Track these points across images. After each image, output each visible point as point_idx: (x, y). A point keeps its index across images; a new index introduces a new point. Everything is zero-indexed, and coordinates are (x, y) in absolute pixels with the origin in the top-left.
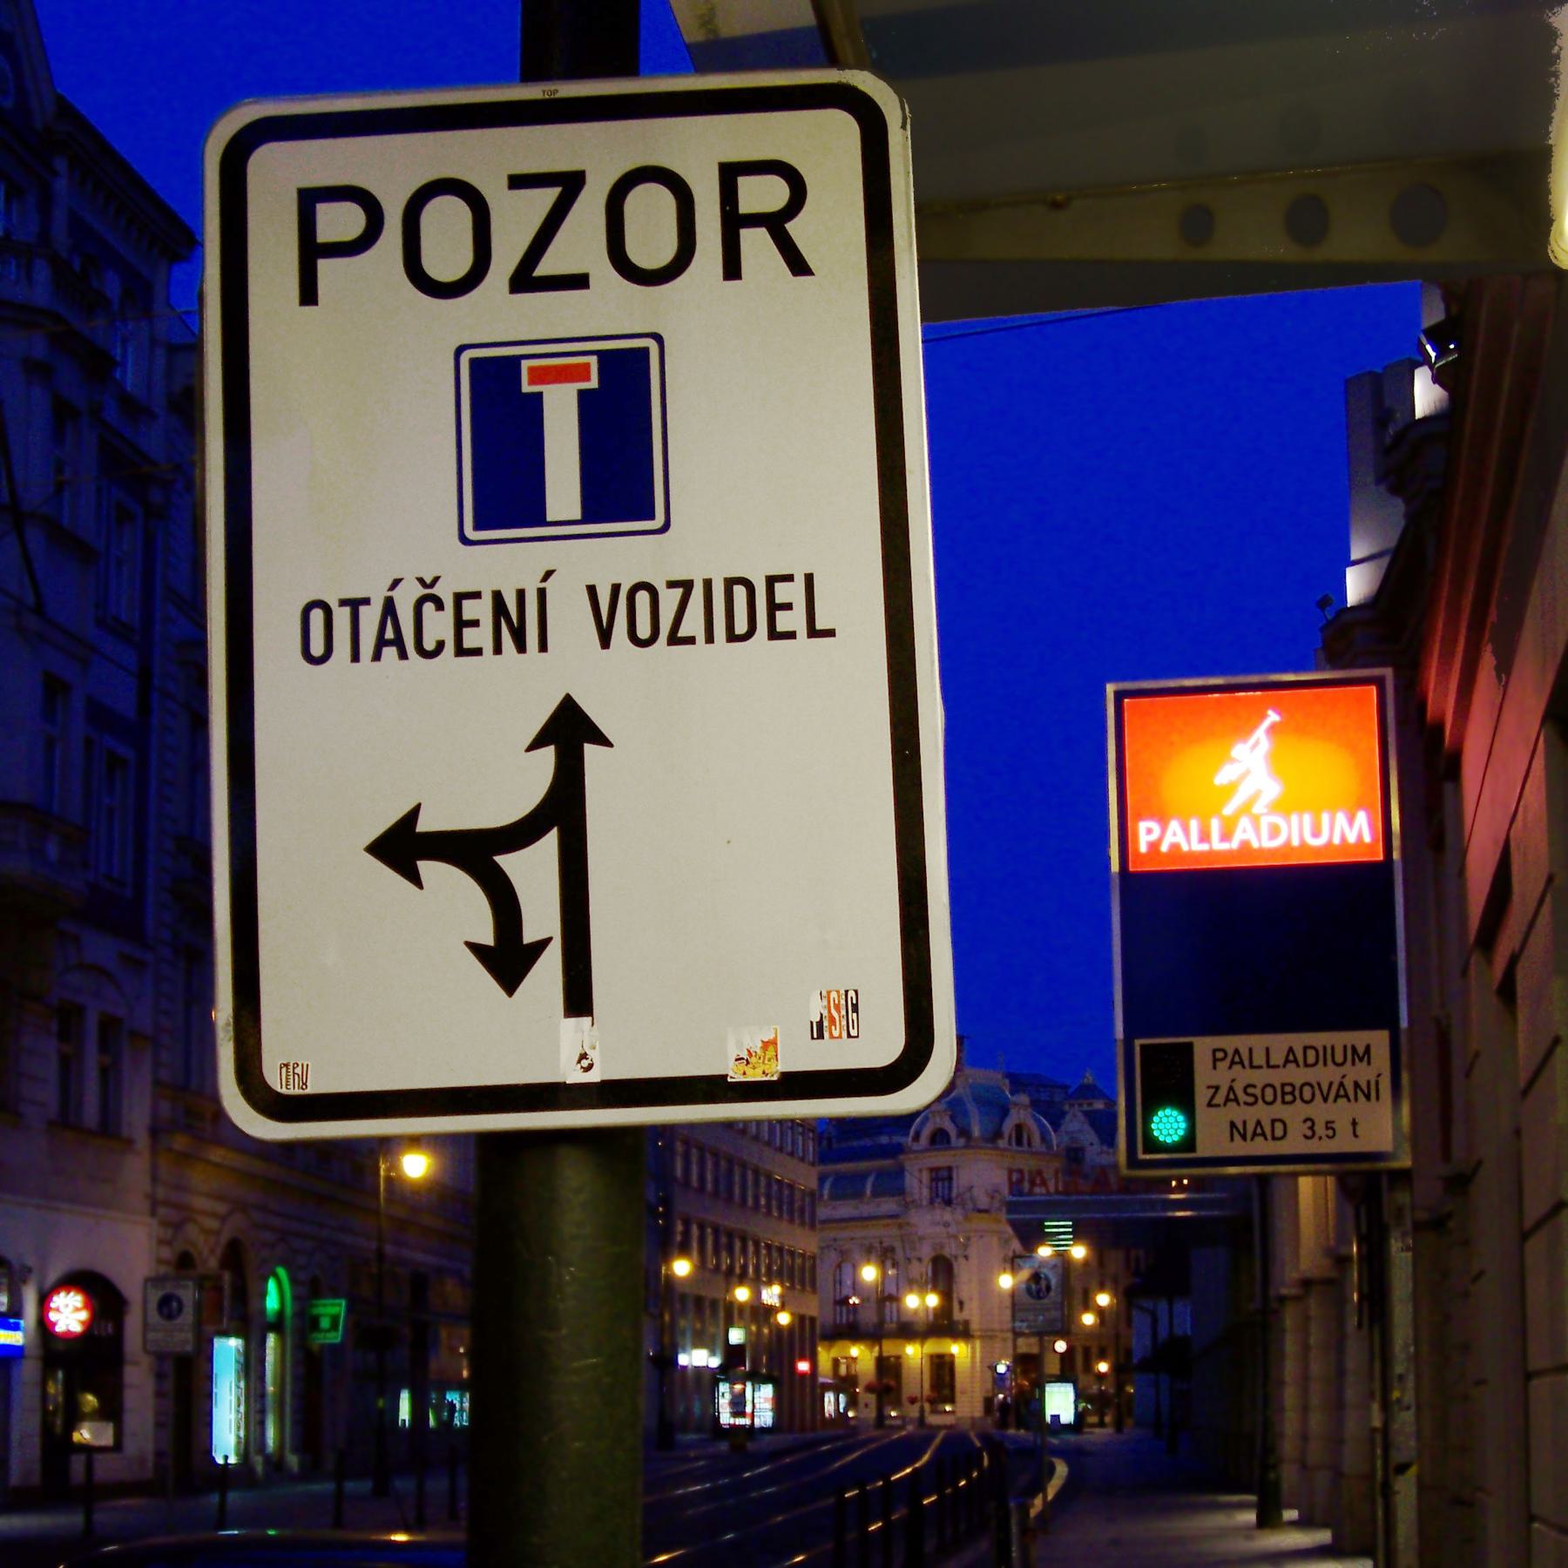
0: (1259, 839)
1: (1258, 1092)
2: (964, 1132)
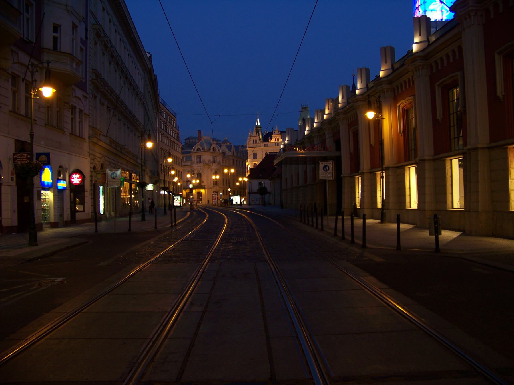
2: (203, 149)
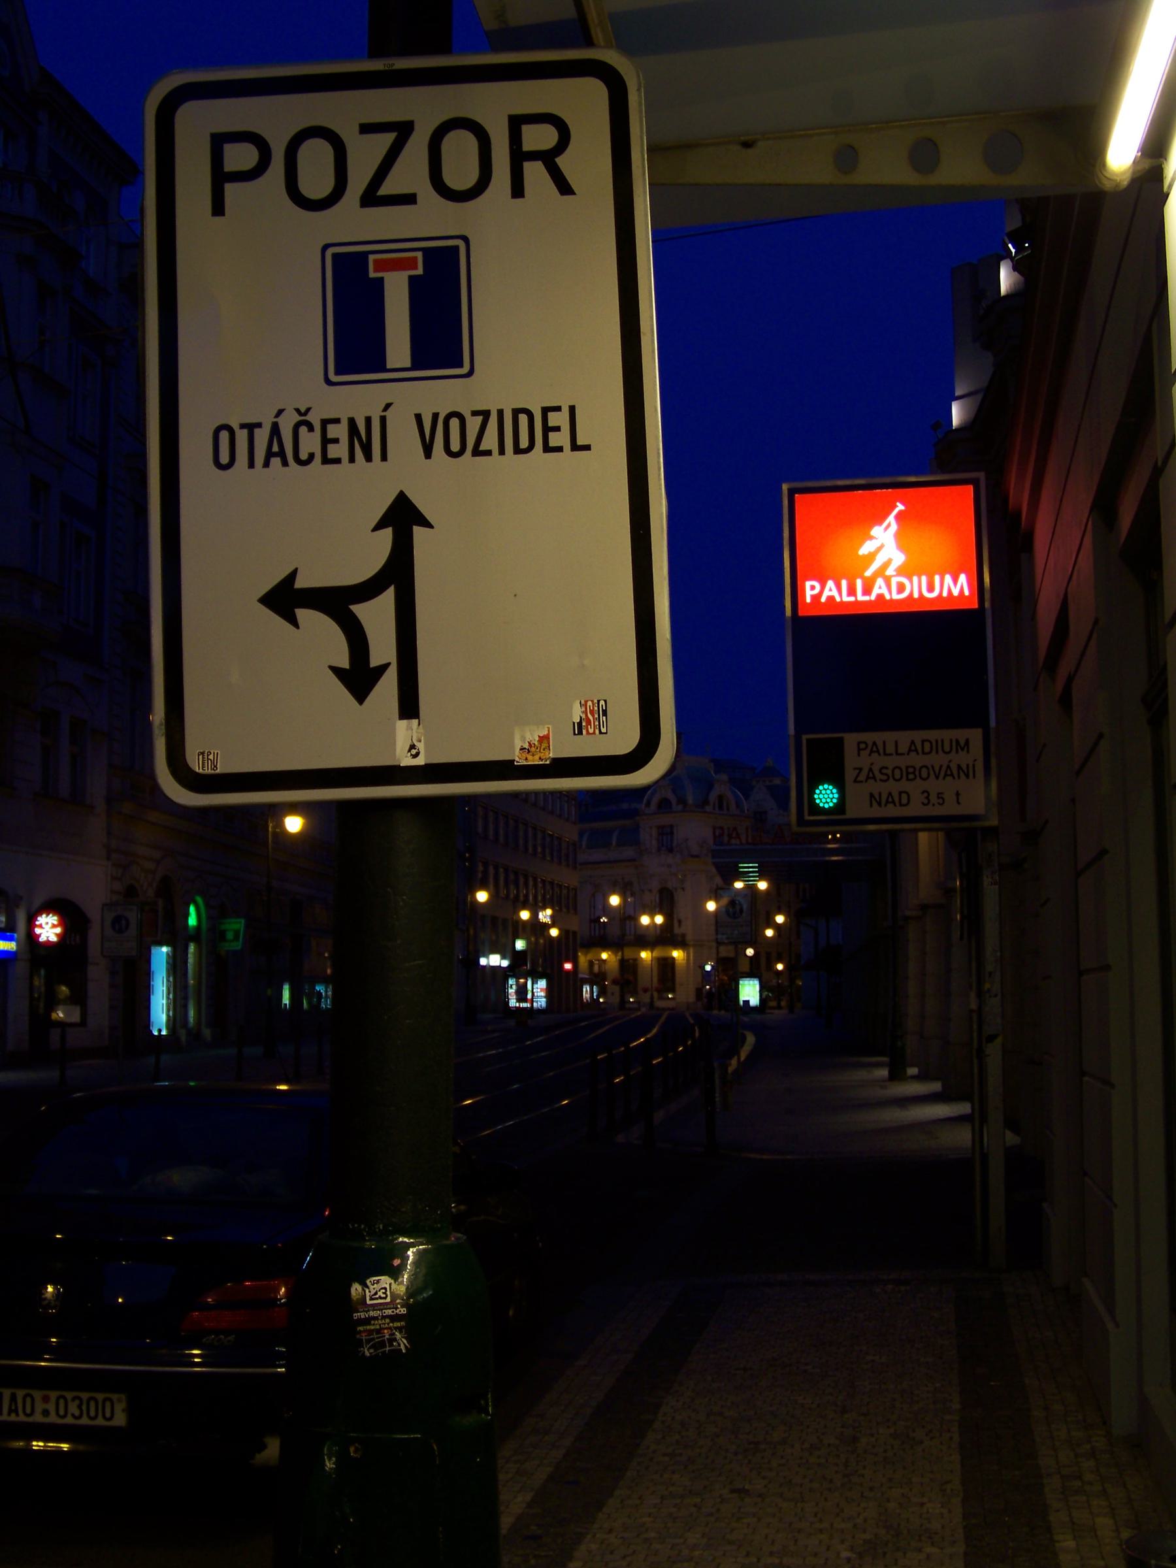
1: (889, 772)
2: (682, 801)
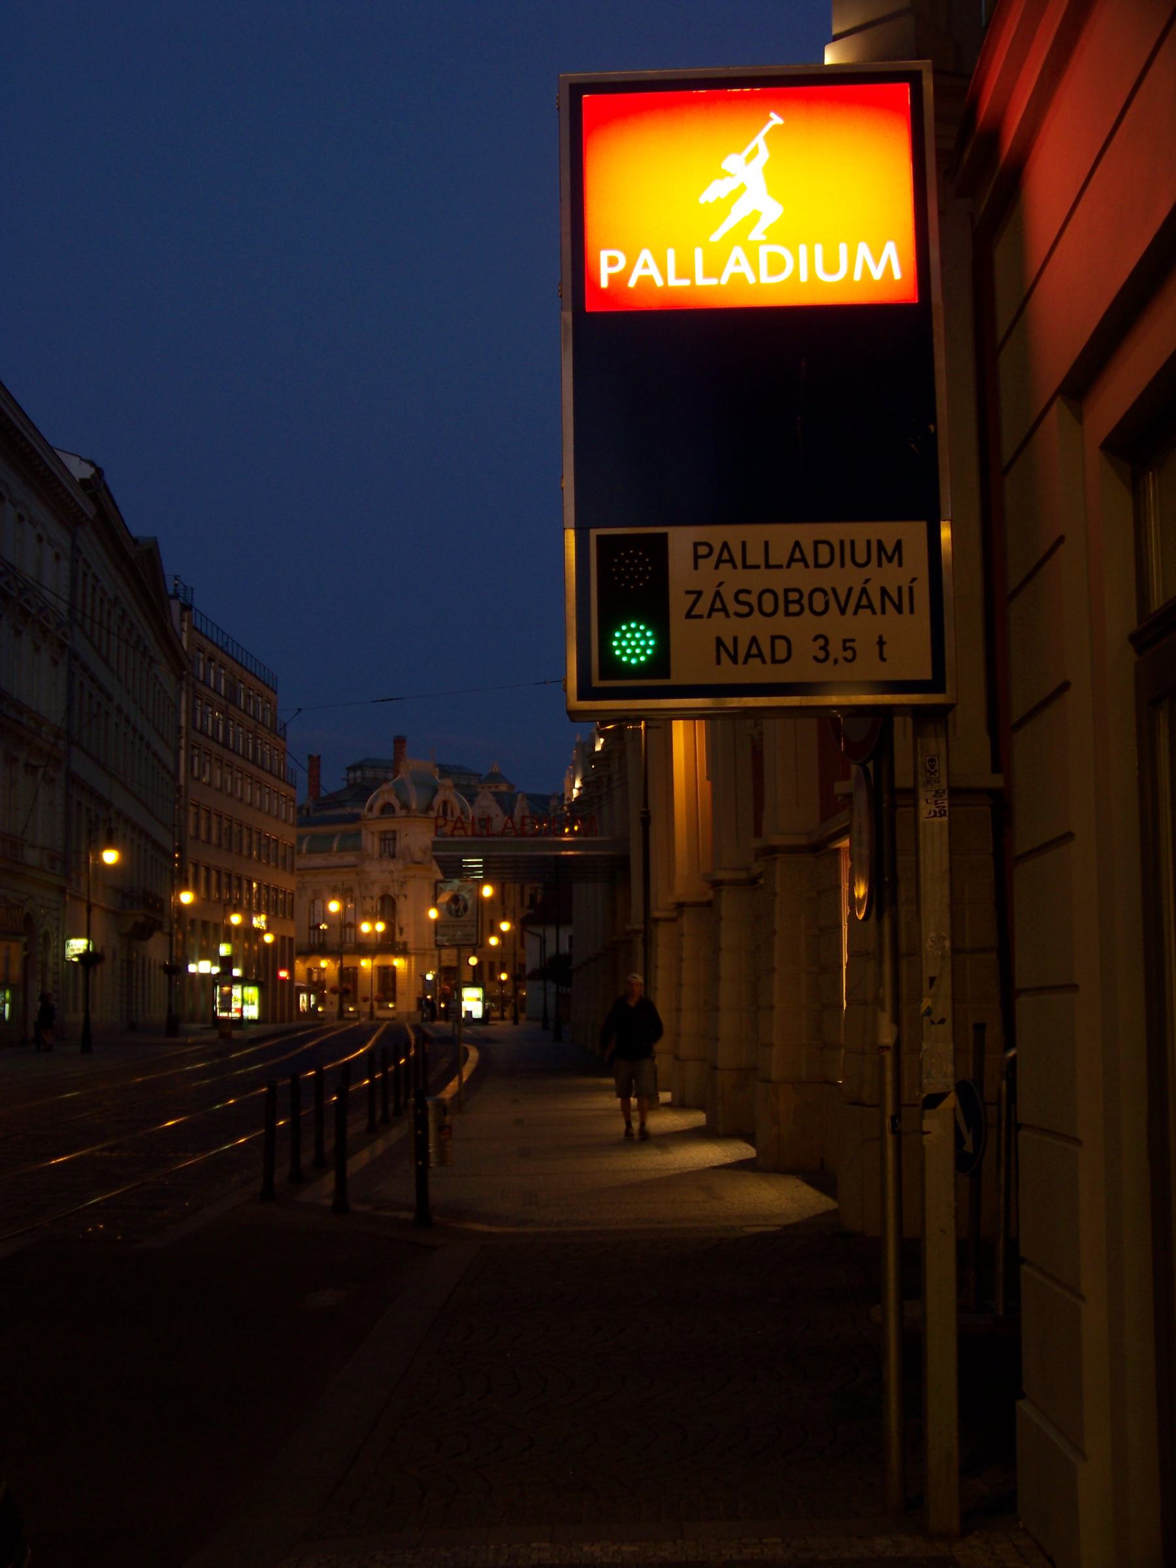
0: (757, 275)
1: (753, 599)
2: (405, 806)
